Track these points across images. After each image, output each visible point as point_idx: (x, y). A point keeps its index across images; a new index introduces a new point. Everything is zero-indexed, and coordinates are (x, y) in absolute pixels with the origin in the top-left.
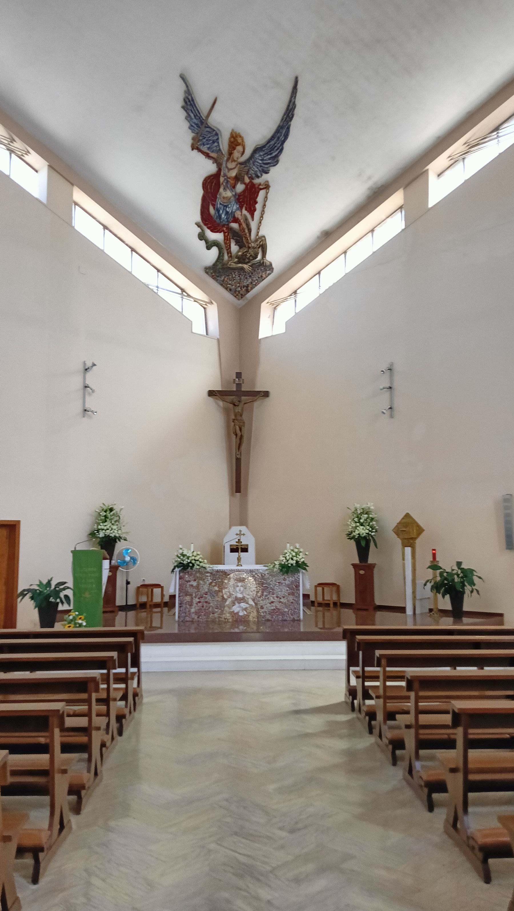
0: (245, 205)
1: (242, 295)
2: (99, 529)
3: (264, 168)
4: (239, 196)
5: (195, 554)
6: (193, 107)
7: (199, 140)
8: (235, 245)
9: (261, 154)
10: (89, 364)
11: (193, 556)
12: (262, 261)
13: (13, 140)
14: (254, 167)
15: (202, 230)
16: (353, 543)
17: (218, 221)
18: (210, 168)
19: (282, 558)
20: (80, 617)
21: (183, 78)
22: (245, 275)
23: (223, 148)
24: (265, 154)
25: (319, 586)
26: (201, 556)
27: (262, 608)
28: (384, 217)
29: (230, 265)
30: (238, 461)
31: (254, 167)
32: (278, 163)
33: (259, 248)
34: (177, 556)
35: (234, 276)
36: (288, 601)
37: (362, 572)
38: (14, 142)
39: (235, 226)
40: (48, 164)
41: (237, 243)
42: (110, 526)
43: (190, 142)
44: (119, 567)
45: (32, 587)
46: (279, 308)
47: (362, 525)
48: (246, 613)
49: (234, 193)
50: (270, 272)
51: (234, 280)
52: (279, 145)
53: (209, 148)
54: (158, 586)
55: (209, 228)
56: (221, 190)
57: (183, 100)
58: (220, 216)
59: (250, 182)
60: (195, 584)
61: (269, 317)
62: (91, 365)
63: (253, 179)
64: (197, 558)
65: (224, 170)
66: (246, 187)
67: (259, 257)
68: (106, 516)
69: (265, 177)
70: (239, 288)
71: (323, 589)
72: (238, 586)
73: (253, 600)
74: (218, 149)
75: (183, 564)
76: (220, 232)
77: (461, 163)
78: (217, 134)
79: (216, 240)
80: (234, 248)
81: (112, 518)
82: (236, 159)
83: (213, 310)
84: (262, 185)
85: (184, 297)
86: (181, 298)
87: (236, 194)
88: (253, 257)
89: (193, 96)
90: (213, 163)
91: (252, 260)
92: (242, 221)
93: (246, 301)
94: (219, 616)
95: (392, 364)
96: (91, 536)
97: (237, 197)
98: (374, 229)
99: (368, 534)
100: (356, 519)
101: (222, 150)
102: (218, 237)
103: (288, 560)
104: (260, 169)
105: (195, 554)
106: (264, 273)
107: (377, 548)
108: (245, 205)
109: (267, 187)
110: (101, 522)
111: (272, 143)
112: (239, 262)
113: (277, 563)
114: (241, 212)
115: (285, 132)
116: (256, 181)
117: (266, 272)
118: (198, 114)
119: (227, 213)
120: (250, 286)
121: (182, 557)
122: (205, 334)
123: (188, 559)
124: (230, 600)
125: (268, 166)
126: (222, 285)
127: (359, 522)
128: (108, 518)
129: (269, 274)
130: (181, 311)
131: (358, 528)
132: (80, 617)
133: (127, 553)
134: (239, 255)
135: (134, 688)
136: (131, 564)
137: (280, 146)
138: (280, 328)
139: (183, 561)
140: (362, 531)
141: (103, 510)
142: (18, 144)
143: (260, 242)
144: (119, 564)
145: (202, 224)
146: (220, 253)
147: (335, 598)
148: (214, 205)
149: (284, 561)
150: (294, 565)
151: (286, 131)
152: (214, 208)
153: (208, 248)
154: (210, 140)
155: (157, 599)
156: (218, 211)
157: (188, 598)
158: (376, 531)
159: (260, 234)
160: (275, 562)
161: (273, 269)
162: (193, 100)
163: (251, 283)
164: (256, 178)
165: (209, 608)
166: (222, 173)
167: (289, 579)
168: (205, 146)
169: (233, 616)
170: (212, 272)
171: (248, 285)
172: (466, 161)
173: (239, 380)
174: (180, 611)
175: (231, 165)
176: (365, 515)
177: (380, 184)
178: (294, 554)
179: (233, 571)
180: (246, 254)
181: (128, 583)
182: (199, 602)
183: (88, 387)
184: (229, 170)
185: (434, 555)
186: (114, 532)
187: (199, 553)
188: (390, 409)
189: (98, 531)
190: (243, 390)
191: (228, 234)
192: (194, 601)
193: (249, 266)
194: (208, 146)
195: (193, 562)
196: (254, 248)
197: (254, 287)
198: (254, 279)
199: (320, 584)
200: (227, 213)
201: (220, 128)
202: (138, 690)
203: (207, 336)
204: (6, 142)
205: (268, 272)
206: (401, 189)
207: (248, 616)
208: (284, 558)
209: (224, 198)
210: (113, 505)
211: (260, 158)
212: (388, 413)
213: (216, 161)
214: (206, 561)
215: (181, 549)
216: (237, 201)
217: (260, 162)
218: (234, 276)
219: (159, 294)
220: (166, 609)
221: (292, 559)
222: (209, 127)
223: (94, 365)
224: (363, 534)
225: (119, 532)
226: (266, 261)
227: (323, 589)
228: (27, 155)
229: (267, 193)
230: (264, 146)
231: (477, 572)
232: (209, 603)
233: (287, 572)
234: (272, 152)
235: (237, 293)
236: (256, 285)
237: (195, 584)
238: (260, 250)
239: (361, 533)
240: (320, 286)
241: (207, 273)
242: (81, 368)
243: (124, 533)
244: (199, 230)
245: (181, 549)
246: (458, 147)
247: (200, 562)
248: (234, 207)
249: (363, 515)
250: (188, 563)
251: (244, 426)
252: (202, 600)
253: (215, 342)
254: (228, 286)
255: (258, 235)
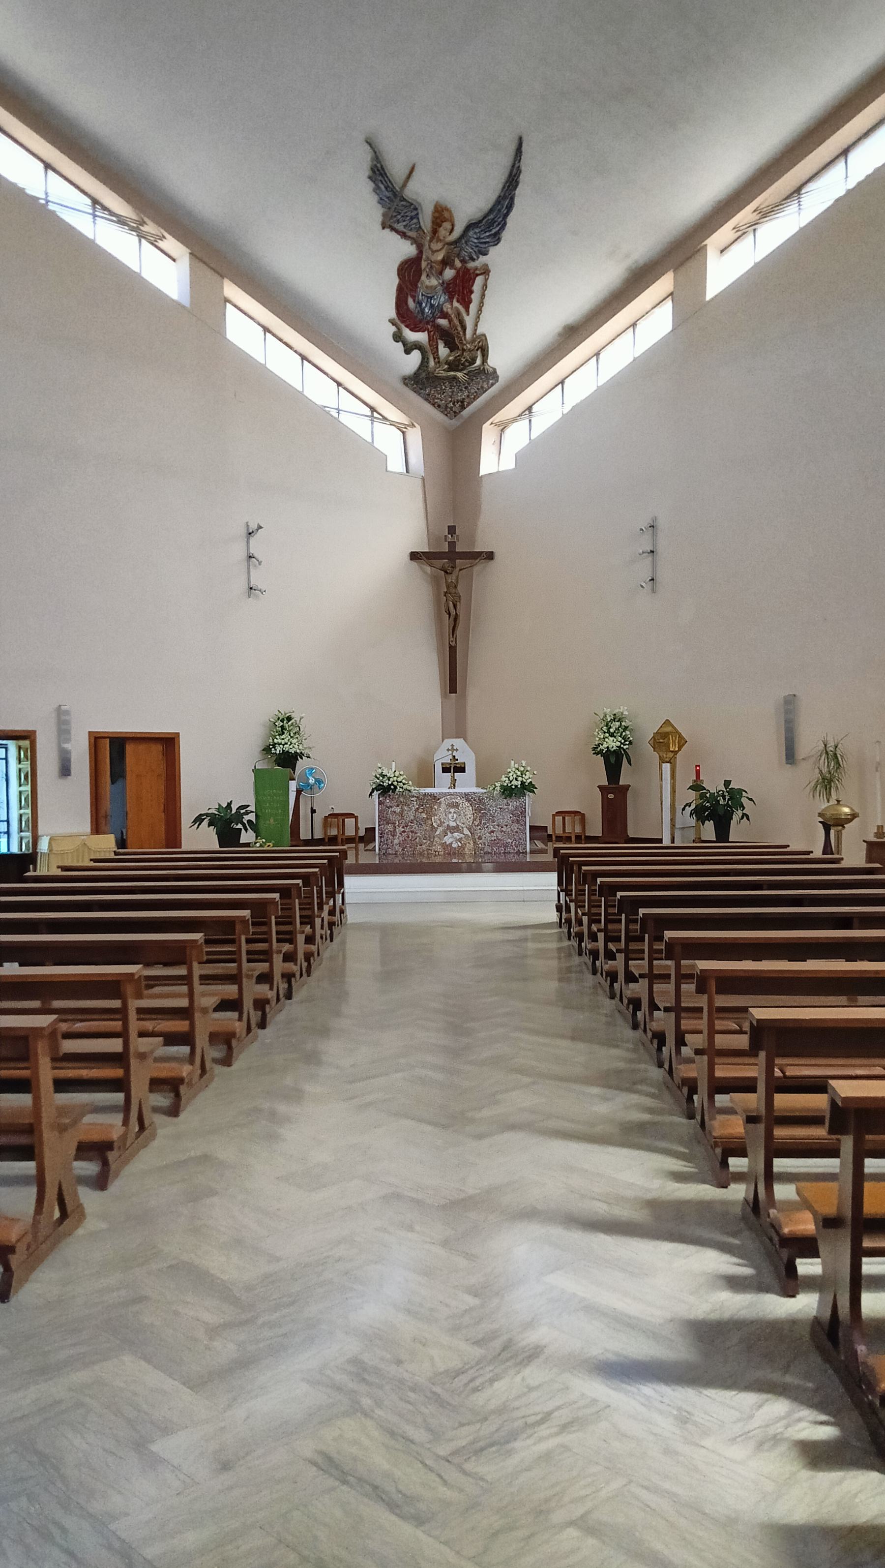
0: (457, 296)
1: (455, 412)
2: (276, 744)
3: (480, 249)
4: (448, 284)
5: (397, 774)
6: (384, 178)
7: (392, 217)
8: (444, 347)
9: (477, 231)
10: (253, 526)
11: (395, 776)
12: (482, 368)
13: (143, 223)
14: (467, 248)
15: (399, 329)
16: (600, 759)
17: (420, 316)
18: (407, 249)
19: (505, 779)
20: (268, 844)
21: (369, 143)
22: (460, 386)
23: (425, 227)
24: (482, 231)
25: (558, 814)
26: (405, 776)
27: (480, 838)
28: (649, 307)
29: (438, 374)
30: (453, 650)
31: (467, 248)
32: (500, 241)
33: (477, 350)
34: (376, 777)
35: (444, 387)
36: (511, 830)
37: (611, 796)
38: (145, 226)
39: (443, 322)
40: (190, 251)
41: (447, 345)
42: (288, 740)
43: (380, 219)
44: (302, 791)
45: (210, 811)
46: (508, 431)
47: (612, 735)
48: (460, 845)
49: (441, 282)
50: (494, 381)
51: (444, 392)
52: (500, 219)
53: (405, 226)
54: (351, 815)
55: (407, 326)
56: (423, 277)
57: (369, 169)
58: (422, 311)
59: (462, 267)
60: (398, 810)
61: (493, 444)
62: (256, 527)
63: (466, 262)
64: (399, 780)
65: (426, 252)
66: (458, 272)
67: (478, 362)
68: (282, 727)
69: (482, 259)
70: (451, 403)
71: (564, 819)
72: (451, 813)
73: (469, 830)
74: (418, 226)
75: (383, 786)
76: (424, 331)
77: (751, 236)
78: (416, 209)
79: (418, 341)
80: (443, 351)
81: (290, 729)
82: (442, 238)
83: (415, 436)
84: (480, 270)
85: (375, 420)
86: (370, 422)
87: (443, 283)
88: (469, 362)
89: (383, 164)
90: (412, 244)
91: (468, 366)
92: (453, 316)
93: (462, 421)
94: (428, 848)
95: (655, 519)
96: (265, 752)
97: (445, 285)
98: (637, 323)
99: (620, 747)
100: (605, 729)
101: (423, 227)
102: (421, 337)
103: (511, 782)
104: (476, 249)
105: (397, 774)
106: (485, 383)
107: (631, 765)
108: (457, 296)
109: (486, 272)
110: (277, 734)
111: (491, 216)
112: (450, 369)
113: (498, 784)
114: (452, 304)
115: (508, 204)
116: (471, 265)
117: (489, 382)
118: (389, 184)
119: (432, 306)
120: (467, 400)
121: (381, 778)
122: (405, 472)
123: (389, 780)
124: (440, 829)
125: (487, 245)
126: (426, 400)
127: (609, 732)
128: (286, 729)
129: (493, 385)
130: (370, 440)
131: (607, 740)
132: (268, 844)
133: (311, 774)
134: (451, 360)
135: (340, 906)
136: (316, 786)
137: (502, 221)
138: (508, 463)
139: (383, 783)
140: (612, 743)
141: (279, 719)
142: (150, 228)
143: (479, 342)
144: (301, 787)
145: (399, 322)
146: (423, 358)
147: (578, 830)
148: (414, 297)
149: (507, 781)
150: (519, 786)
151: (509, 202)
152: (414, 301)
153: (408, 351)
154: (407, 216)
155: (350, 832)
156: (420, 304)
157: (390, 827)
158: (631, 743)
159: (478, 332)
160: (496, 783)
161: (498, 377)
162: (383, 169)
163: (468, 396)
164: (470, 261)
165: (416, 839)
166: (424, 257)
167: (514, 803)
168: (400, 224)
169: (444, 849)
170: (412, 382)
171: (464, 399)
172: (758, 233)
173: (452, 536)
174: (381, 842)
175: (436, 246)
176: (617, 723)
177: (641, 262)
178: (519, 773)
179: (445, 795)
180: (460, 359)
181: (313, 811)
182: (404, 832)
183: (254, 557)
184: (434, 252)
185: (698, 773)
186: (294, 747)
187: (402, 773)
188: (652, 581)
189: (274, 745)
190: (457, 551)
191: (434, 333)
192: (397, 830)
193: (465, 374)
194: (405, 223)
195: (395, 783)
196: (470, 350)
197: (472, 402)
198: (473, 391)
199: (559, 813)
200: (432, 306)
201: (420, 200)
202: (343, 907)
203: (408, 474)
204: (135, 225)
205: (491, 381)
206: (668, 273)
207: (463, 847)
208: (507, 779)
209: (427, 287)
210: (290, 712)
211: (475, 236)
212: (648, 587)
213: (414, 241)
214: (410, 782)
215: (380, 768)
216: (445, 291)
217: (476, 241)
218: (444, 387)
219: (341, 419)
220: (361, 846)
221: (516, 780)
222: (404, 200)
223: (260, 527)
224: (613, 747)
225: (301, 747)
226: (488, 367)
227: (564, 819)
228: (162, 240)
229: (486, 280)
230: (480, 221)
231: (746, 792)
232: (416, 833)
233: (510, 796)
234: (491, 228)
235: (449, 410)
236: (475, 399)
237: (398, 810)
238: (479, 352)
239: (611, 747)
240: (563, 404)
241: (406, 384)
242: (243, 531)
243: (306, 748)
244: (393, 329)
245: (380, 768)
246: (745, 215)
247: (404, 784)
248: (441, 298)
249: (613, 723)
250: (389, 785)
251: (460, 602)
252: (407, 829)
253: (419, 482)
254: (436, 401)
255: (475, 334)
